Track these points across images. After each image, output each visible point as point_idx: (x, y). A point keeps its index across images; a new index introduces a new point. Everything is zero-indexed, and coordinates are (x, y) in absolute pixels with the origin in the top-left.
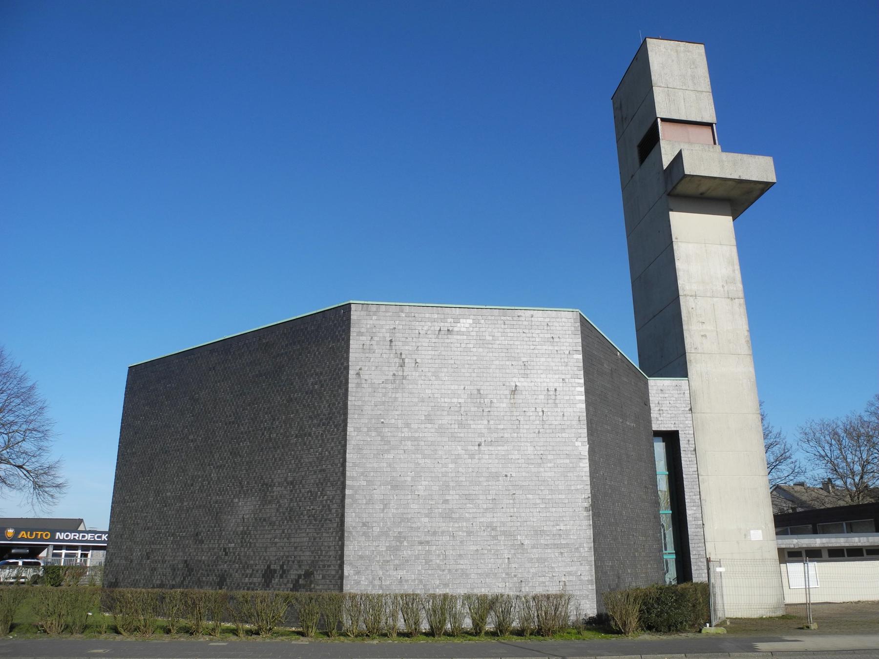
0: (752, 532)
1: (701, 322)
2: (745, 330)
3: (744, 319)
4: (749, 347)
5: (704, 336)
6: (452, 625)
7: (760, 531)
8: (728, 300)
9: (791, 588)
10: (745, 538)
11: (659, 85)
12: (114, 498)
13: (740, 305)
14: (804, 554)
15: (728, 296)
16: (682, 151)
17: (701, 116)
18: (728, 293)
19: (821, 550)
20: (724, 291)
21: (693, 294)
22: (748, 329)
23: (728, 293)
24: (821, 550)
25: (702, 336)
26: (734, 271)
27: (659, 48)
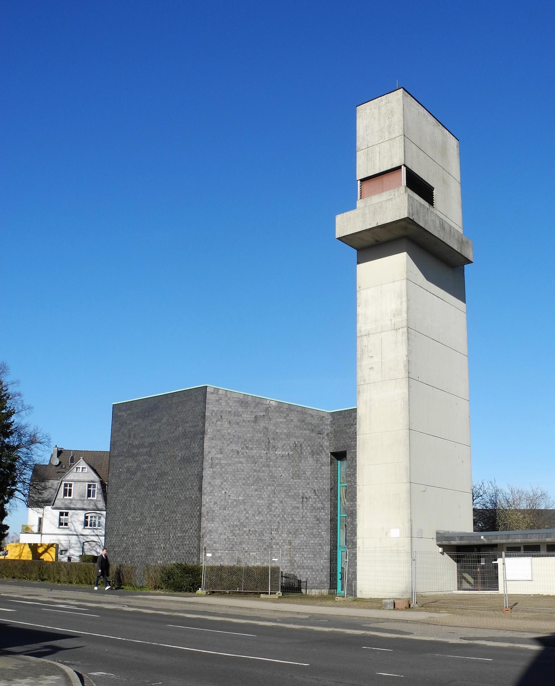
0: (392, 530)
1: (371, 357)
2: (404, 356)
3: (404, 346)
4: (406, 370)
5: (371, 368)
6: (464, 601)
7: (398, 530)
8: (394, 332)
9: (530, 578)
10: (386, 535)
11: (361, 149)
12: (490, 530)
13: (403, 333)
14: (522, 549)
15: (394, 327)
16: (426, 204)
17: (391, 163)
18: (394, 325)
19: (539, 546)
20: (391, 324)
21: (367, 333)
22: (357, 352)
23: (394, 325)
24: (539, 546)
25: (370, 368)
26: (401, 303)
27: (365, 111)
